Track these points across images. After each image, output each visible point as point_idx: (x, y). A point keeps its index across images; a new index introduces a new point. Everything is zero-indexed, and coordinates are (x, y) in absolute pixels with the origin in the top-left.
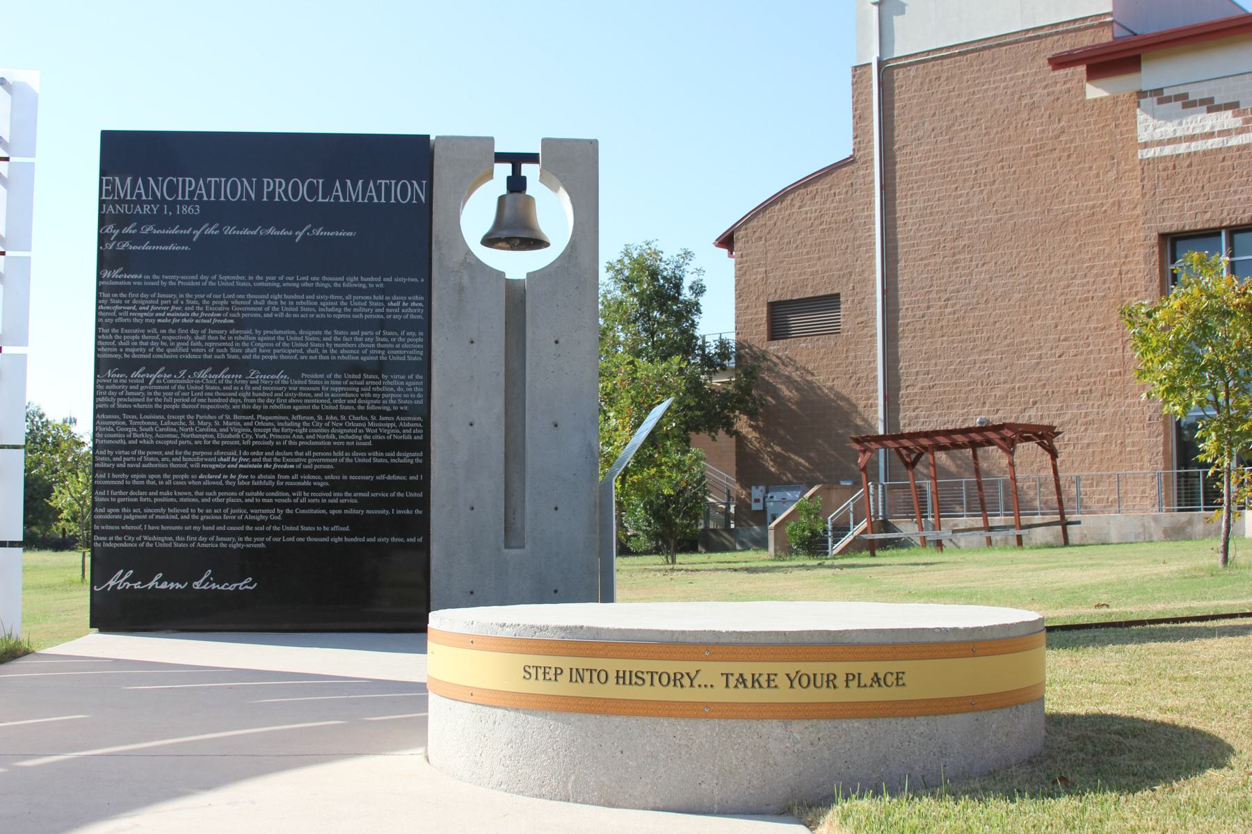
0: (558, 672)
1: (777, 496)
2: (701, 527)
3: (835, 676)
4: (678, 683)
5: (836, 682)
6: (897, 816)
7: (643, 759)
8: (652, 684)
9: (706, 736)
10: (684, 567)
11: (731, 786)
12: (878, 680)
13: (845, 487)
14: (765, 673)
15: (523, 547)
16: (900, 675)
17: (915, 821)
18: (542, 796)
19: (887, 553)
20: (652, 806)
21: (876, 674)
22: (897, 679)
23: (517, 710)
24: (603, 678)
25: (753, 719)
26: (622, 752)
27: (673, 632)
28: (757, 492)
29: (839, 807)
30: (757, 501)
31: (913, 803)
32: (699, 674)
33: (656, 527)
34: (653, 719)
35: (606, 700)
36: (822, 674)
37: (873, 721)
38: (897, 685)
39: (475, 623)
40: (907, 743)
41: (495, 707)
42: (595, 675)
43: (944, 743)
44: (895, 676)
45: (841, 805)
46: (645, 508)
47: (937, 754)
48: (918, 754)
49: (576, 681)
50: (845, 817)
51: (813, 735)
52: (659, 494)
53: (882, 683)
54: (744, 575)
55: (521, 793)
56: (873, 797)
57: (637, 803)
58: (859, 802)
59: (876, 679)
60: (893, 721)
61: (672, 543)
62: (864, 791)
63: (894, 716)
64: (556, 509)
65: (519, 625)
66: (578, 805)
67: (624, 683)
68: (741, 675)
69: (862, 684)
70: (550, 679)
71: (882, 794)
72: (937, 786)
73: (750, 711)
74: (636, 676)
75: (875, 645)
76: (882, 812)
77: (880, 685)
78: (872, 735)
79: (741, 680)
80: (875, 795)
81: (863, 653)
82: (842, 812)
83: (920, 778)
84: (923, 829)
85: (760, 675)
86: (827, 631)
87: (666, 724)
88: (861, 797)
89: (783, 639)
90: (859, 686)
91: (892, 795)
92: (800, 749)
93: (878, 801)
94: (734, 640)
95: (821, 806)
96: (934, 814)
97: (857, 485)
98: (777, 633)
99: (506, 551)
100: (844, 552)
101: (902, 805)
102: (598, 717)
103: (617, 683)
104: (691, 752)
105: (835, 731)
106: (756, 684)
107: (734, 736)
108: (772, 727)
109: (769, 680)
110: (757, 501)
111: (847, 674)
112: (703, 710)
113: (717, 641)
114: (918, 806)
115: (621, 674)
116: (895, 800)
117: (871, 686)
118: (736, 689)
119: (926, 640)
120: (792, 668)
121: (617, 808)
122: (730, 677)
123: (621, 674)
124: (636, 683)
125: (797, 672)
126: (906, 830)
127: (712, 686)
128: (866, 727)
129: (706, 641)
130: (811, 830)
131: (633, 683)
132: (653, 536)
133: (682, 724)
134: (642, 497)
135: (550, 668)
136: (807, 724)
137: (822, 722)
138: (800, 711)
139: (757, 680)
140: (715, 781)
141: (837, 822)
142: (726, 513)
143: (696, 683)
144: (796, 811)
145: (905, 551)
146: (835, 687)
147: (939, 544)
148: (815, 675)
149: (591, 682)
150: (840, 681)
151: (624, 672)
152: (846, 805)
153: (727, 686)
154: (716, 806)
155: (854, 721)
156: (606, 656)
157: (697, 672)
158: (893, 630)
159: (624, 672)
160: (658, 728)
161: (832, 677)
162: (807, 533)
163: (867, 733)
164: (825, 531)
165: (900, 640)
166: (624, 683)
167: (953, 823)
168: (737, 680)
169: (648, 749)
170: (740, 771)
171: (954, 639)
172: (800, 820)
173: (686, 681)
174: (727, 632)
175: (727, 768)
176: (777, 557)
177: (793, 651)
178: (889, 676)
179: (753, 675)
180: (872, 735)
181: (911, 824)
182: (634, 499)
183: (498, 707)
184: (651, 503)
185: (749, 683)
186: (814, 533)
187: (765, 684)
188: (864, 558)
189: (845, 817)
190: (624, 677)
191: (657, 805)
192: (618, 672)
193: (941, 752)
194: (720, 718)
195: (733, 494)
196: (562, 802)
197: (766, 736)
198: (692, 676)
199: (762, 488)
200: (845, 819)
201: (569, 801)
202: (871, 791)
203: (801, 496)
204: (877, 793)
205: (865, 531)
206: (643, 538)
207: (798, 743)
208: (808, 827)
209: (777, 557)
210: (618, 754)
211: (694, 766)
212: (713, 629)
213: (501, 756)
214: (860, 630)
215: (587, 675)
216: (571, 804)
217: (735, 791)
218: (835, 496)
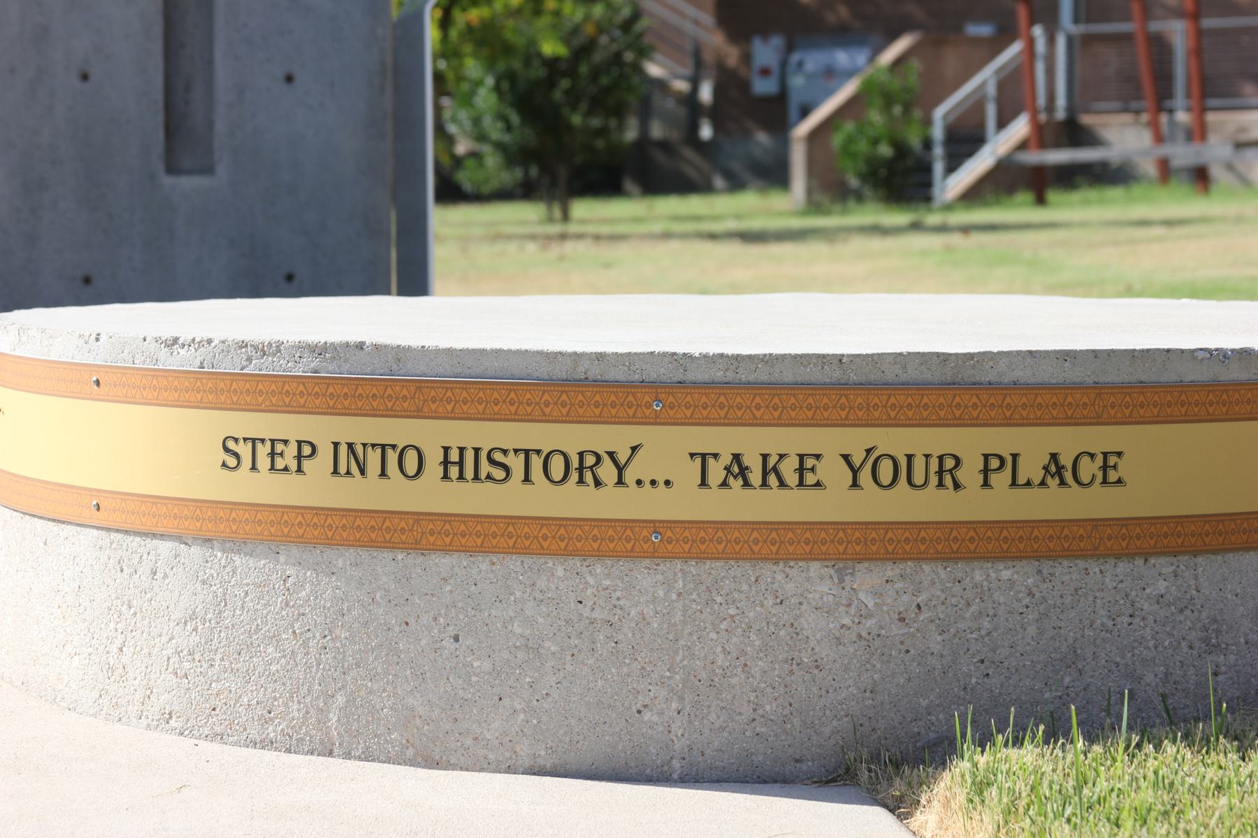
0: (306, 451)
1: (813, 60)
2: (631, 134)
3: (958, 461)
4: (588, 477)
5: (959, 474)
6: (1102, 785)
7: (505, 655)
8: (527, 479)
9: (654, 599)
10: (591, 229)
11: (713, 717)
12: (1060, 469)
13: (977, 41)
14: (793, 451)
15: (208, 170)
16: (1112, 460)
17: (1147, 795)
18: (267, 744)
19: (1076, 196)
20: (527, 764)
21: (1054, 457)
22: (1105, 468)
23: (208, 541)
24: (411, 467)
25: (765, 559)
26: (456, 639)
27: (577, 357)
28: (766, 52)
29: (966, 765)
30: (765, 72)
31: (1140, 756)
32: (640, 454)
33: (526, 135)
34: (528, 560)
35: (418, 516)
36: (927, 456)
37: (1046, 567)
38: (1105, 481)
39: (103, 338)
40: (1126, 619)
41: (154, 536)
42: (392, 457)
43: (1215, 621)
44: (1099, 460)
45: (971, 759)
46: (497, 89)
47: (1197, 644)
48: (1151, 644)
49: (348, 473)
50: (980, 787)
51: (905, 598)
52: (531, 55)
53: (1068, 476)
54: (735, 249)
55: (219, 737)
56: (1047, 742)
57: (491, 757)
58: (1013, 752)
59: (1054, 468)
60: (1094, 567)
61: (563, 172)
62: (1025, 730)
63: (1098, 557)
64: (289, 79)
65: (210, 341)
66: (353, 764)
67: (461, 477)
68: (737, 457)
69: (1021, 480)
70: (286, 469)
71: (1067, 734)
72: (1197, 720)
73: (756, 542)
74: (492, 461)
75: (1052, 388)
76: (1066, 776)
77: (1063, 483)
78: (1044, 599)
79: (736, 469)
80: (1050, 737)
81: (1024, 406)
82: (974, 775)
83: (1157, 700)
84: (1166, 813)
85: (782, 456)
86: (938, 355)
87: (560, 572)
88: (1018, 742)
89: (836, 374)
90: (1014, 483)
91: (1091, 739)
92: (875, 632)
93: (1058, 752)
94: (719, 375)
95: (924, 762)
96: (1190, 780)
97: (1005, 35)
98: (823, 359)
99: (168, 181)
100: (973, 195)
101: (1114, 760)
102: (400, 557)
103: (446, 476)
104: (620, 637)
105: (957, 588)
106: (773, 480)
107: (719, 599)
108: (808, 579)
109: (801, 470)
110: (765, 72)
111: (986, 457)
112: (647, 540)
113: (679, 376)
114: (1152, 764)
115: (454, 456)
116: (1098, 749)
117: (1043, 483)
118: (725, 491)
119: (1173, 377)
120: (856, 440)
121: (446, 769)
122: (711, 461)
123: (454, 456)
124: (489, 477)
125: (869, 451)
126: (1125, 814)
127: (667, 483)
128: (1030, 581)
129: (653, 377)
130: (902, 817)
131: (483, 475)
132: (514, 156)
133: (599, 574)
134: (490, 65)
135: (286, 442)
136: (889, 573)
137: (927, 568)
138: (873, 541)
139: (775, 469)
140: (674, 705)
141: (961, 798)
142: (690, 100)
143: (630, 476)
144: (864, 776)
145: (1116, 192)
146: (957, 486)
147: (1201, 177)
148: (910, 457)
149: (383, 474)
150: (970, 474)
151: (462, 450)
152: (982, 760)
153: (704, 483)
154: (676, 764)
155: (1001, 566)
156: (418, 414)
157: (634, 449)
158: (1095, 354)
159: (462, 450)
160: (542, 583)
161: (949, 463)
162: (885, 150)
163: (1031, 594)
164: (928, 144)
165: (1111, 377)
166: (461, 477)
167: (1235, 801)
168: (728, 469)
169: (518, 630)
170: (734, 681)
171: (1244, 376)
172: (873, 796)
173: (607, 472)
174: (705, 357)
175: (704, 675)
176: (813, 206)
177: (859, 400)
178: (1085, 460)
179: (765, 457)
180: (1044, 599)
181: (1137, 803)
182: (472, 67)
183: (162, 537)
184: (511, 76)
185: (755, 477)
186: (901, 150)
187: (792, 478)
188: (1020, 210)
189: (980, 787)
190: (461, 464)
191: (541, 761)
192: (446, 450)
193: (1206, 641)
194: (686, 557)
195: (708, 57)
196: (314, 758)
197: (794, 600)
198: (622, 460)
199: (777, 41)
200: (981, 793)
201: (330, 754)
202: (1042, 727)
203: (872, 58)
204: (1056, 732)
205: (1023, 146)
206: (492, 160)
207: (870, 616)
208: (892, 811)
209: (813, 206)
210: (448, 643)
211: (625, 670)
212: (671, 349)
213: (169, 652)
214: (1019, 353)
215: (374, 458)
216: (336, 763)
217: (722, 729)
218: (951, 59)
